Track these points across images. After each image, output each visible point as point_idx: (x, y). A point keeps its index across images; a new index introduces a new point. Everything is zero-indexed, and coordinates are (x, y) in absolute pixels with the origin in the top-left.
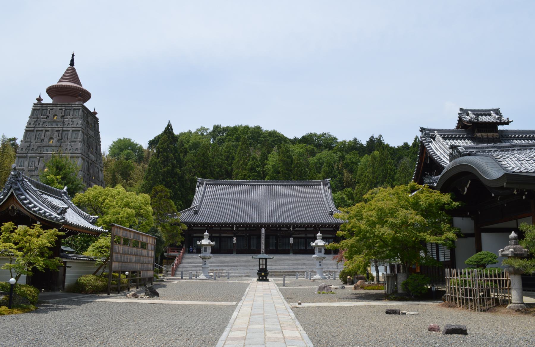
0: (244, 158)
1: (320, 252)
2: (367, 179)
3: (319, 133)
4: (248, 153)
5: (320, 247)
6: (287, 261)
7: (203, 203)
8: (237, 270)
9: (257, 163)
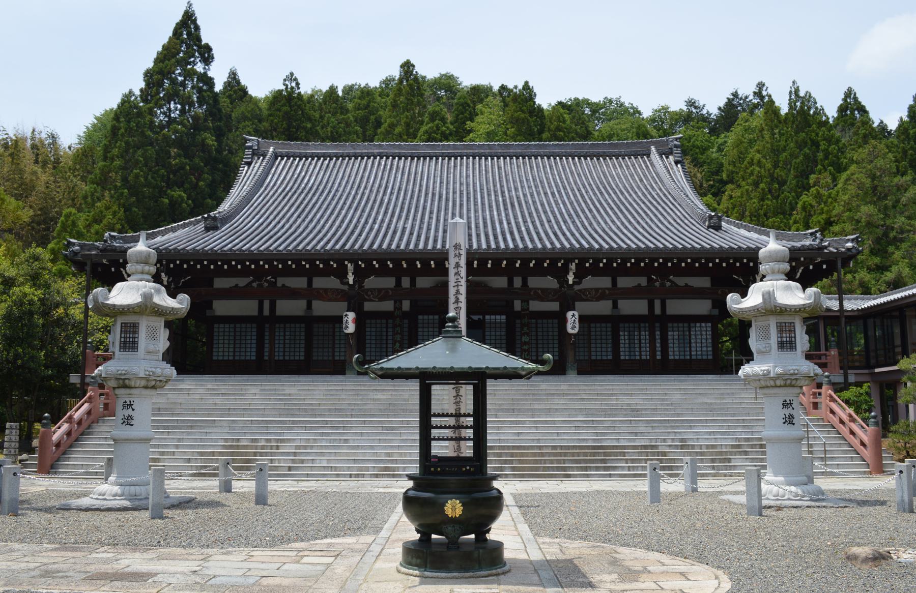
0: (407, 117)
1: (787, 345)
2: (758, 169)
3: (596, 97)
4: (419, 104)
5: (786, 319)
6: (561, 402)
7: (252, 202)
8: (346, 441)
9: (444, 128)
